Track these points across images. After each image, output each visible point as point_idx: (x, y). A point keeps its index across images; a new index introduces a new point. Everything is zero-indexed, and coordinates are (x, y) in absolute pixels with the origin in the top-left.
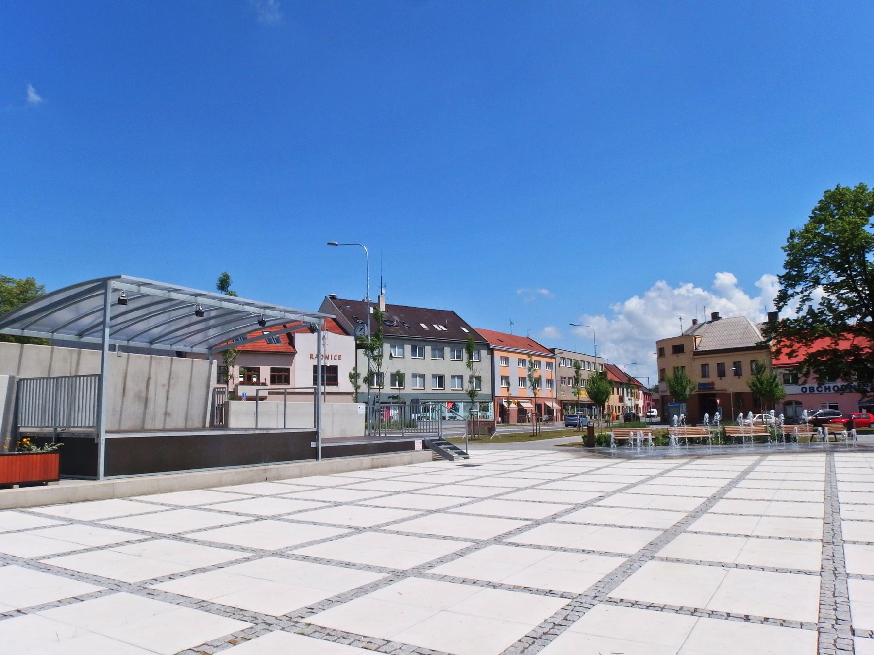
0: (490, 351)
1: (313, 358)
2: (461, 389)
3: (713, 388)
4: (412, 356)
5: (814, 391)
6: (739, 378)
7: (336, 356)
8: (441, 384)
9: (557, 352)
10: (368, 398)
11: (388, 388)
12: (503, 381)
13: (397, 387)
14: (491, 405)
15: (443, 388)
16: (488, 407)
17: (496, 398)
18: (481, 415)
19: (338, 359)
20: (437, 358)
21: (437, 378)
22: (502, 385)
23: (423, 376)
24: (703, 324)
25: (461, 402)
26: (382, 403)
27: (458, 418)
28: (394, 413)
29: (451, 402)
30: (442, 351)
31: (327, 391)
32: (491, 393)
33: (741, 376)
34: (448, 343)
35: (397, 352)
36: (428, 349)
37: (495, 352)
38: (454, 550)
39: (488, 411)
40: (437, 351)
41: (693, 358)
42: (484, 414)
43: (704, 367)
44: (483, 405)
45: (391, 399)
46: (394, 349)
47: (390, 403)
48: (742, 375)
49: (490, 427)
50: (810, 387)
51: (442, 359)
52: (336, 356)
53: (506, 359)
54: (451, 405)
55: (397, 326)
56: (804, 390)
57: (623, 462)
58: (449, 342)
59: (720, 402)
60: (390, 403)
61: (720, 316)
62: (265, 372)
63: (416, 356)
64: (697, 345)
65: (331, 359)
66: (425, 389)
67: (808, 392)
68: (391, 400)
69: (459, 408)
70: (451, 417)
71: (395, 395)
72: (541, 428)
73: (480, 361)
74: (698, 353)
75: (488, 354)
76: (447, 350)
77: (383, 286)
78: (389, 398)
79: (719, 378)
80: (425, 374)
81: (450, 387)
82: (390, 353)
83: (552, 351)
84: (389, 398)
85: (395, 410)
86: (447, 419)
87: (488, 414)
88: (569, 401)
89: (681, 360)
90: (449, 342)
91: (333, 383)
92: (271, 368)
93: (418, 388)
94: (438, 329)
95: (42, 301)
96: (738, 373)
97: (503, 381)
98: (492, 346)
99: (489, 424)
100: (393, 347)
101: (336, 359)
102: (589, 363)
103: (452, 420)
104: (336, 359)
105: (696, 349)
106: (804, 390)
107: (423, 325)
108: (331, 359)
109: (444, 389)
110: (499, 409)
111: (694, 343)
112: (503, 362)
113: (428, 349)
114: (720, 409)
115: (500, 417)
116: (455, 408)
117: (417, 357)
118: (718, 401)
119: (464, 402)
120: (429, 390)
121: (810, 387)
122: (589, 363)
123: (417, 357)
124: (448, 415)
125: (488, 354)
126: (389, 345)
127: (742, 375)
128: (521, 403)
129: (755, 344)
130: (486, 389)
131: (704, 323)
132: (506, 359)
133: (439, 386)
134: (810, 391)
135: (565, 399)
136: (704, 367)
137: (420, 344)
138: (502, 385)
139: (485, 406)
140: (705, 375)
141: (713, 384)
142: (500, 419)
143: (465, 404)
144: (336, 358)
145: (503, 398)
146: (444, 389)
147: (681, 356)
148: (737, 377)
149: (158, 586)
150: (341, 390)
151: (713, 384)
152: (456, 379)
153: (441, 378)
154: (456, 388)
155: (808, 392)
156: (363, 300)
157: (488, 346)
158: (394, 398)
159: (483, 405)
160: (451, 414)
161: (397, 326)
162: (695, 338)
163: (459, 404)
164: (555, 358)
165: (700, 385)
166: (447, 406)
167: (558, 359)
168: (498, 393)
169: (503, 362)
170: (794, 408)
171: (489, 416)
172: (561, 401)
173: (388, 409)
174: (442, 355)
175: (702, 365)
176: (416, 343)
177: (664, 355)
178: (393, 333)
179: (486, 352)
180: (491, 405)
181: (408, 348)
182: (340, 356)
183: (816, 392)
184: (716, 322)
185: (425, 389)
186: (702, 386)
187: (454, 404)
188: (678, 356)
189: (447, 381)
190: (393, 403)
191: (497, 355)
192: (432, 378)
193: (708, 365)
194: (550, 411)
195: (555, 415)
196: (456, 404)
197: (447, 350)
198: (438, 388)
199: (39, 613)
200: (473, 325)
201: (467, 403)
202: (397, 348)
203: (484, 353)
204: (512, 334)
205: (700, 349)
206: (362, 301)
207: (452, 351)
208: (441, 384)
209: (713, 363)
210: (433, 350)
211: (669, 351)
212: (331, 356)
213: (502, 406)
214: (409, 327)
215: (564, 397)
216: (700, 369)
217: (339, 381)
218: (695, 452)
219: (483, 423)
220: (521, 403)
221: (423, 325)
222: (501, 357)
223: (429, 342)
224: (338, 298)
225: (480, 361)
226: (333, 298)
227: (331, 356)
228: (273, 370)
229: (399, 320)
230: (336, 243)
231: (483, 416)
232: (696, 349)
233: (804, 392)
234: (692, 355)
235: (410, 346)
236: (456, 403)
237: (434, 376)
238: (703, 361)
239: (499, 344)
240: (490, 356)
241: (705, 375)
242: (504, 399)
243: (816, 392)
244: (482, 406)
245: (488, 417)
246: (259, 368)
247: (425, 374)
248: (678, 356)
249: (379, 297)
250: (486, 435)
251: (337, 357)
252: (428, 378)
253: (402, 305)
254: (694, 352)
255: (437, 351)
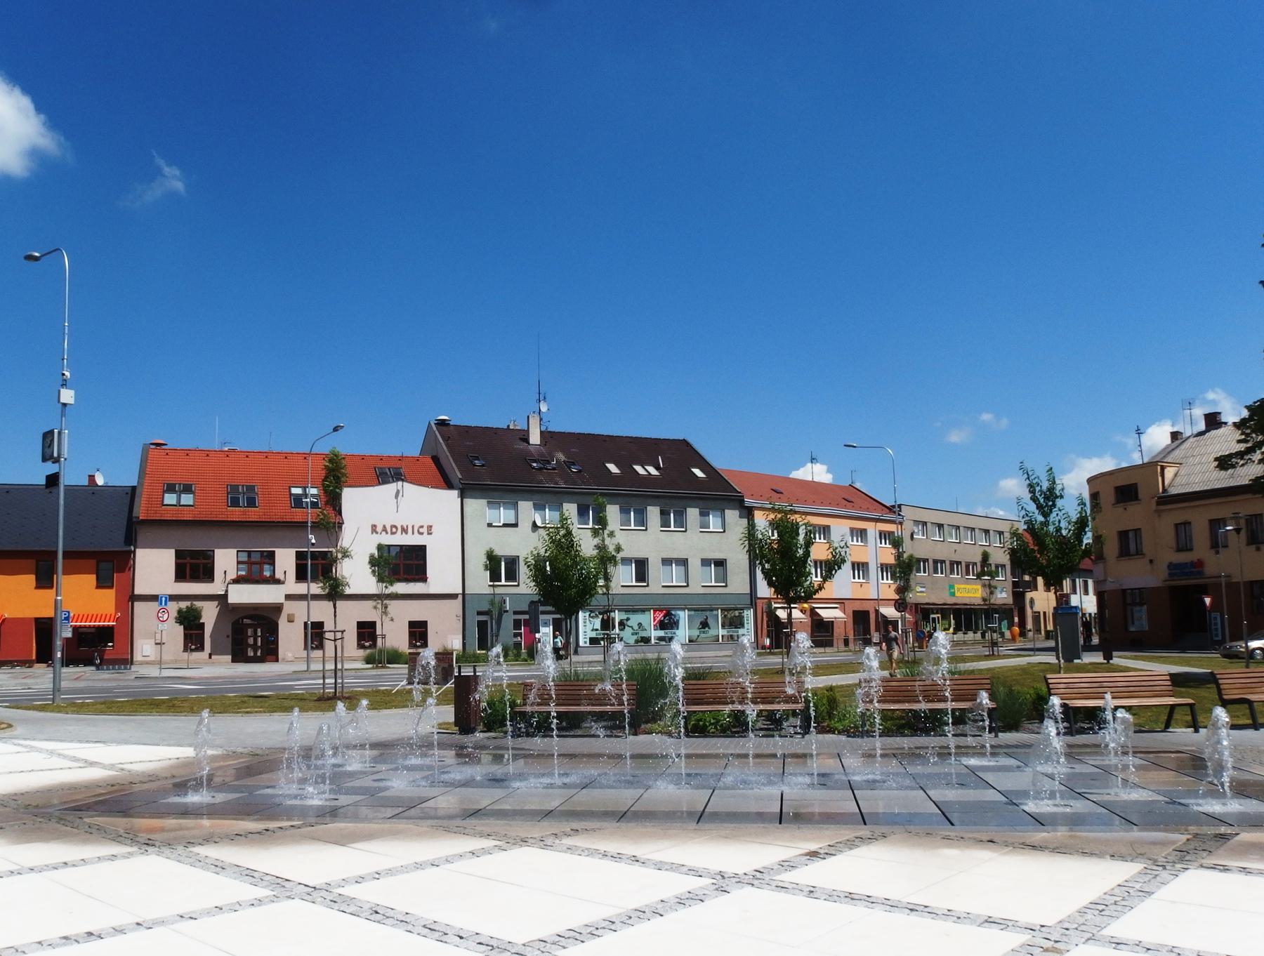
0: (745, 512)
1: (377, 533)
2: (685, 584)
3: (1201, 573)
7: (422, 527)
9: (905, 511)
10: (56, 600)
12: (856, 572)
13: (503, 582)
14: (749, 615)
16: (741, 618)
21: (634, 565)
22: (854, 578)
23: (683, 562)
24: (1189, 437)
25: (683, 609)
29: (661, 611)
31: (312, 592)
32: (749, 592)
34: (654, 499)
38: (700, 885)
39: (742, 625)
40: (632, 513)
41: (1155, 511)
42: (733, 632)
43: (1182, 529)
51: (644, 528)
52: (422, 527)
54: (660, 616)
55: (554, 469)
57: (131, 854)
58: (658, 497)
59: (1212, 602)
61: (1223, 420)
62: (286, 560)
64: (1167, 483)
65: (413, 533)
66: (688, 586)
69: (678, 621)
70: (661, 639)
72: (321, 681)
73: (724, 532)
74: (1168, 500)
75: (741, 517)
77: (542, 398)
79: (1213, 551)
81: (662, 580)
83: (894, 509)
86: (653, 641)
89: (1133, 516)
90: (658, 497)
91: (417, 577)
92: (297, 552)
95: (888, 525)
97: (856, 572)
98: (749, 501)
100: (539, 507)
101: (422, 534)
102: (987, 532)
104: (422, 534)
105: (1164, 490)
108: (413, 533)
109: (648, 586)
110: (767, 622)
111: (1160, 479)
112: (855, 538)
113: (653, 513)
114: (1215, 618)
115: (768, 636)
118: (1208, 600)
119: (689, 610)
120: (696, 588)
124: (655, 634)
125: (741, 517)
126: (530, 504)
128: (817, 610)
135: (927, 601)
136: (1182, 529)
138: (854, 578)
139: (735, 616)
140: (1184, 545)
141: (1200, 564)
142: (768, 642)
143: (693, 613)
144: (421, 530)
146: (648, 586)
147: (1133, 508)
149: (349, 891)
150: (432, 591)
151: (1200, 564)
152: (674, 565)
156: (508, 426)
160: (661, 633)
161: (554, 469)
162: (1163, 468)
164: (901, 523)
169: (855, 538)
172: (916, 605)
175: (1177, 525)
176: (589, 500)
178: (541, 482)
179: (737, 513)
180: (749, 615)
182: (430, 527)
184: (1213, 433)
185: (688, 586)
187: (668, 614)
188: (1125, 509)
189: (654, 569)
192: (702, 565)
193: (1190, 523)
196: (672, 614)
199: (171, 926)
200: (717, 463)
204: (814, 480)
205: (1174, 491)
206: (506, 427)
207: (625, 511)
209: (1199, 519)
210: (664, 513)
211: (1108, 497)
212: (413, 527)
214: (580, 471)
215: (923, 597)
216: (1172, 533)
218: (437, 823)
220: (817, 610)
222: (852, 530)
224: (451, 423)
225: (724, 532)
226: (442, 423)
227: (413, 527)
228: (179, 554)
230: (37, 254)
231: (731, 636)
232: (1164, 490)
233: (418, 531)
234: (1155, 504)
236: (673, 612)
238: (1176, 515)
239: (845, 506)
240: (460, 499)
241: (1184, 545)
244: (729, 616)
246: (274, 551)
248: (1125, 509)
249: (528, 417)
251: (424, 530)
252: (695, 564)
253: (582, 432)
254: (1159, 498)
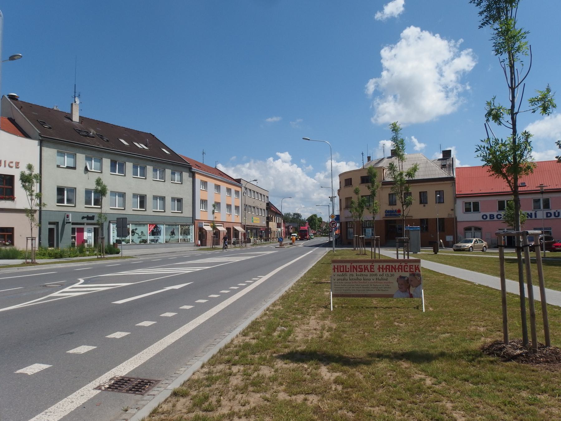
0: (192, 174)
4: (111, 172)
5: (494, 218)
6: (424, 206)
7: (12, 162)
8: (142, 204)
9: (242, 182)
11: (81, 207)
14: (192, 228)
15: (144, 210)
16: (189, 229)
17: (196, 221)
18: (182, 238)
19: (14, 167)
20: (139, 177)
21: (139, 198)
26: (73, 224)
27: (159, 241)
28: (88, 236)
29: (153, 225)
30: (143, 169)
33: (426, 205)
35: (93, 165)
36: (129, 166)
37: (197, 176)
40: (139, 169)
42: (185, 237)
44: (184, 228)
45: (86, 219)
46: (90, 162)
47: (83, 224)
48: (427, 203)
49: (407, 275)
50: (490, 215)
52: (12, 162)
53: (204, 184)
56: (485, 217)
60: (83, 224)
63: (116, 172)
65: (5, 166)
66: (124, 209)
67: (488, 219)
68: (85, 221)
69: (161, 231)
70: (152, 241)
71: (90, 215)
76: (150, 169)
78: (83, 218)
80: (125, 193)
82: (85, 166)
83: (239, 181)
84: (83, 218)
85: (89, 231)
86: (148, 242)
87: (189, 237)
88: (249, 226)
91: (7, 197)
93: (117, 208)
94: (140, 147)
96: (440, 200)
99: (401, 268)
100: (88, 159)
103: (153, 243)
104: (12, 167)
106: (485, 217)
107: (123, 141)
108: (5, 166)
109: (146, 210)
110: (199, 232)
113: (129, 166)
116: (155, 232)
117: (117, 173)
119: (166, 225)
121: (490, 215)
122: (261, 194)
123: (117, 173)
124: (150, 238)
125: (189, 177)
127: (427, 203)
129: (557, 157)
130: (187, 212)
131: (383, 159)
132: (204, 184)
133: (140, 207)
134: (490, 218)
137: (120, 159)
143: (167, 226)
144: (11, 165)
145: (203, 222)
148: (423, 205)
153: (143, 200)
154: (158, 210)
155: (488, 219)
157: (190, 169)
158: (89, 218)
159: (184, 228)
160: (152, 237)
162: (383, 170)
163: (161, 226)
165: (387, 212)
166: (147, 230)
167: (243, 188)
168: (198, 217)
170: (473, 233)
171: (190, 239)
172: (244, 226)
173: (81, 231)
174: (143, 174)
177: (351, 184)
180: (192, 228)
181: (107, 162)
183: (496, 219)
186: (388, 213)
187: (156, 227)
189: (149, 202)
190: (88, 224)
191: (198, 178)
194: (236, 233)
195: (240, 238)
196: (158, 227)
197: (150, 169)
198: (139, 209)
201: (169, 225)
202: (93, 161)
203: (186, 175)
207: (155, 170)
208: (142, 204)
210: (135, 167)
211: (356, 182)
212: (5, 162)
213: (201, 229)
217: (16, 195)
219: (385, 264)
221: (123, 141)
223: (130, 158)
226: (12, 98)
229: (95, 133)
231: (184, 239)
235: (110, 160)
236: (158, 226)
237: (135, 196)
241: (392, 203)
242: (204, 223)
243: (496, 219)
244: (184, 229)
245: (188, 240)
247: (125, 193)
249: (72, 104)
250: (391, 296)
251: (13, 165)
255: (139, 169)
